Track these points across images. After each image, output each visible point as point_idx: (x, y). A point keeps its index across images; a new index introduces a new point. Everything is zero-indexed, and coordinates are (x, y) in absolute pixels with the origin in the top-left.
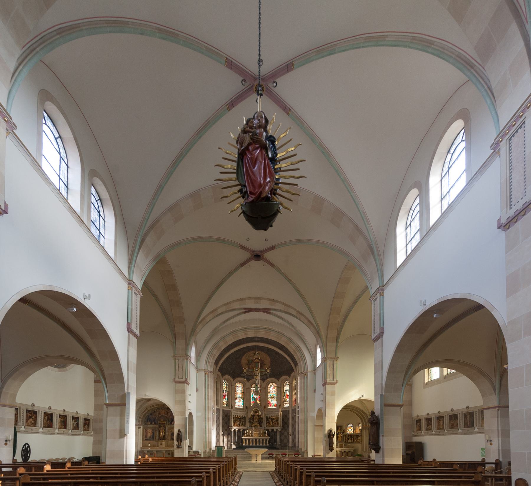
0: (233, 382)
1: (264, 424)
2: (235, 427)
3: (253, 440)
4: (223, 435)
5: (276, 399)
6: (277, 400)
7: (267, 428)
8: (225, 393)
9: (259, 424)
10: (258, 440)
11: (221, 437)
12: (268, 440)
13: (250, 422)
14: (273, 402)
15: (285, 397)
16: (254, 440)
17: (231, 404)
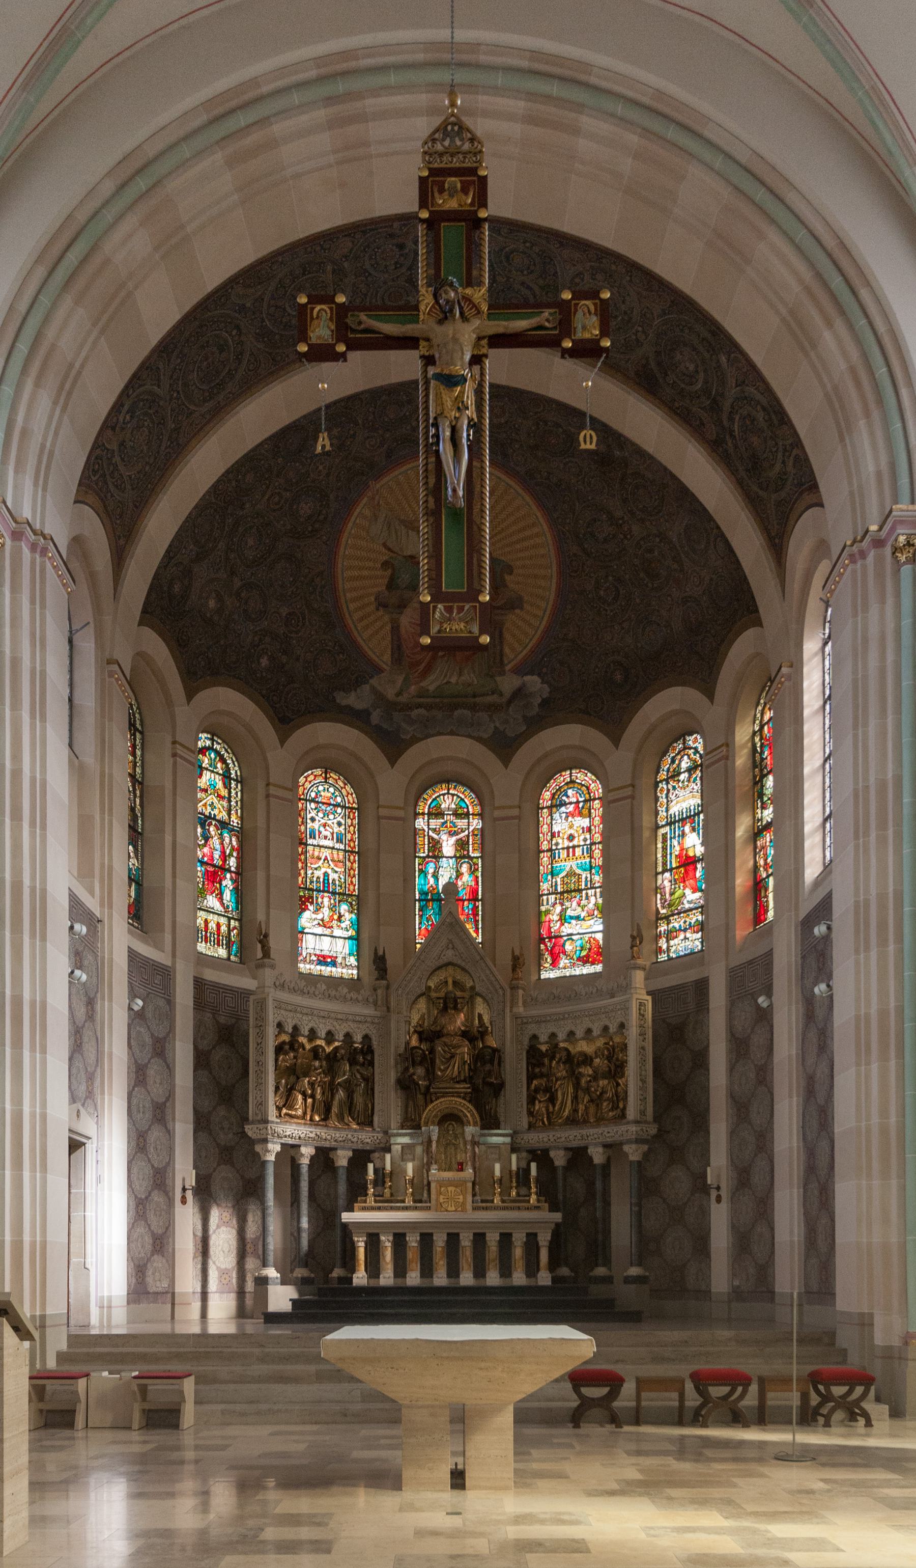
0: (279, 757)
1: (514, 1098)
2: (289, 1131)
3: (426, 1239)
4: (204, 1194)
5: (594, 899)
6: (606, 912)
7: (536, 1139)
8: (218, 846)
9: (476, 1098)
10: (466, 1241)
11: (186, 1218)
12: (544, 1239)
13: (405, 1085)
14: (580, 923)
15: (665, 880)
16: (440, 1241)
17: (256, 941)
